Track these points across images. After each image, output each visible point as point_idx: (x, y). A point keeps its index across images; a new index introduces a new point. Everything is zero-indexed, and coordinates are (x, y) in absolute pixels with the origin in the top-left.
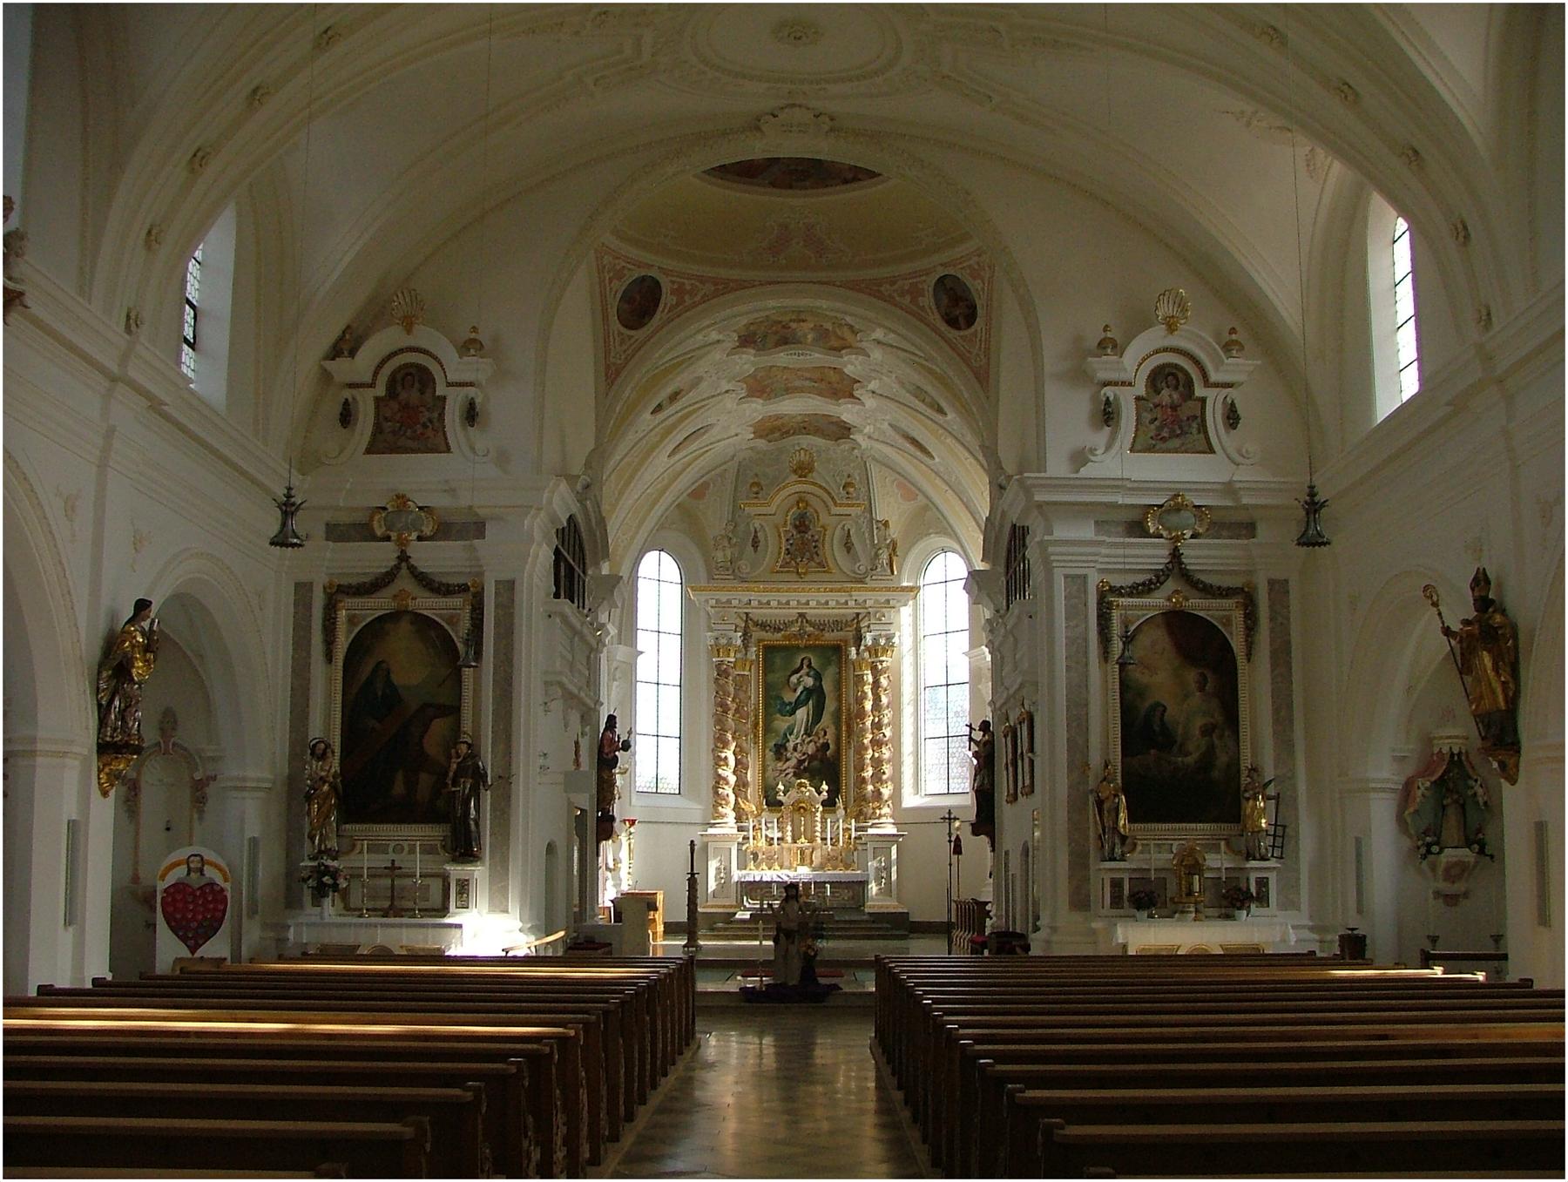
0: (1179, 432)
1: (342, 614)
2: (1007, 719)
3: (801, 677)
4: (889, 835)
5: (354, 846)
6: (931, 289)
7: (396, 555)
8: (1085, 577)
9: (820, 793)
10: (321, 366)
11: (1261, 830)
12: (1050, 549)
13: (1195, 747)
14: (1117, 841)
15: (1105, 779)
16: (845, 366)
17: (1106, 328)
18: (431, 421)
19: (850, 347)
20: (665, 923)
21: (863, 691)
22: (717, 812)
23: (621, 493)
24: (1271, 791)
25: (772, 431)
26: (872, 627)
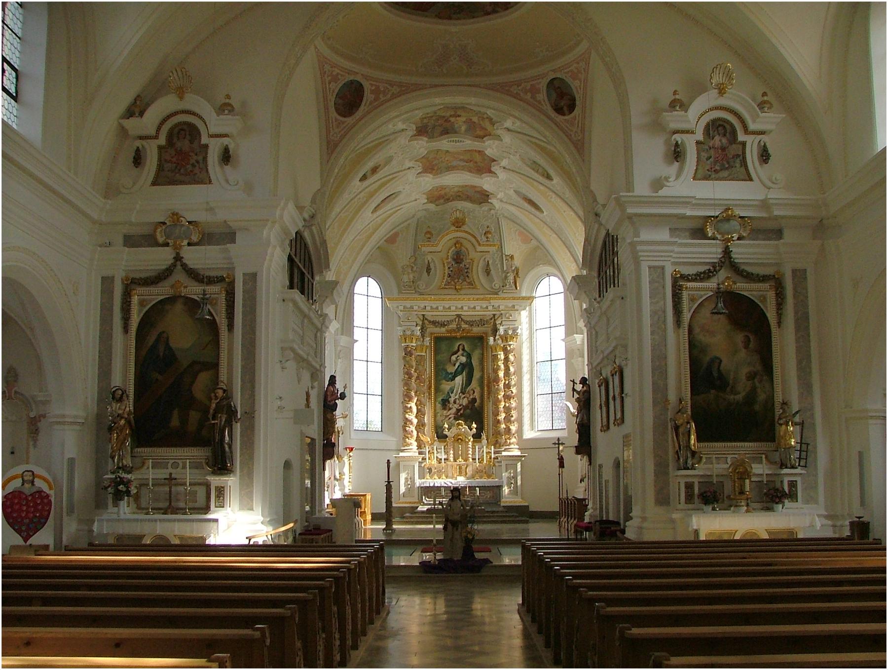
0: (727, 166)
1: (135, 300)
2: (601, 374)
3: (458, 356)
4: (516, 456)
5: (143, 463)
6: (545, 88)
7: (172, 256)
8: (663, 268)
9: (471, 429)
10: (120, 124)
11: (791, 447)
12: (640, 254)
13: (742, 388)
14: (689, 455)
15: (680, 411)
16: (487, 149)
17: (675, 93)
18: (198, 162)
19: (490, 135)
20: (372, 514)
21: (498, 365)
22: (405, 442)
23: (342, 235)
24: (797, 419)
25: (440, 197)
26: (503, 323)
